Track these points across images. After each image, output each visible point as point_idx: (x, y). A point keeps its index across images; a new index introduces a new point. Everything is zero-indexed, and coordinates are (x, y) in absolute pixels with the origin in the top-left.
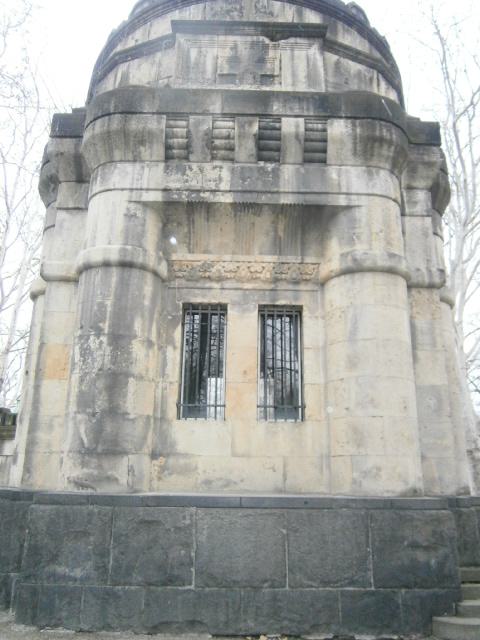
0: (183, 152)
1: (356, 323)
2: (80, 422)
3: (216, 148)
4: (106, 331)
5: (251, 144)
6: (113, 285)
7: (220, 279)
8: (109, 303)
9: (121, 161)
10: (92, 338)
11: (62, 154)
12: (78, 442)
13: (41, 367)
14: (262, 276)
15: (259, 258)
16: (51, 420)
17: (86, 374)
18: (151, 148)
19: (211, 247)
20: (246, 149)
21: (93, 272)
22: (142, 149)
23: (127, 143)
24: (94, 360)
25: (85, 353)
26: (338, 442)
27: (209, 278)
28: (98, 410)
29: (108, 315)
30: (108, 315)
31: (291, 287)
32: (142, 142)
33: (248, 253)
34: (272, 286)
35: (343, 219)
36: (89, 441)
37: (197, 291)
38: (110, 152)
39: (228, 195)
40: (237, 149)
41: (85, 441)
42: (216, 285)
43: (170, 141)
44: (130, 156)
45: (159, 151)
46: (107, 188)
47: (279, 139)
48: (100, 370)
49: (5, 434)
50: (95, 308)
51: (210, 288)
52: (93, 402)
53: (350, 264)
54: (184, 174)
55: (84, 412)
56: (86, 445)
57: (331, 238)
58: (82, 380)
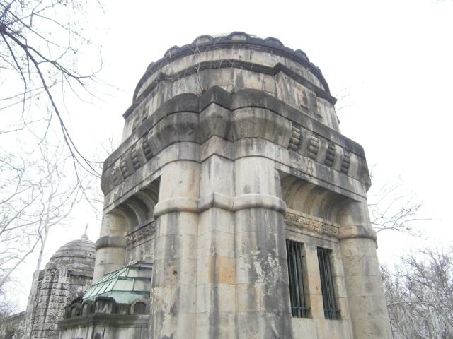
0: (296, 147)
1: (235, 245)
2: (270, 318)
3: (309, 150)
4: (277, 254)
5: (324, 154)
6: (276, 223)
7: (301, 228)
8: (276, 235)
9: (268, 140)
10: (270, 258)
11: (221, 117)
12: (271, 334)
13: (217, 273)
14: (318, 229)
15: (314, 218)
16: (227, 315)
17: (269, 284)
18: (284, 139)
19: (294, 205)
20: (321, 156)
21: (263, 211)
22: (280, 137)
23: (274, 130)
24: (273, 274)
25: (266, 269)
26: (365, 333)
27: (297, 226)
28: (280, 311)
29: (277, 243)
30: (277, 243)
31: (328, 238)
32: (280, 133)
33: (309, 213)
34: (321, 237)
35: (353, 206)
36: (278, 332)
37: (291, 233)
38: (263, 132)
39: (316, 180)
40: (318, 154)
41: (276, 332)
42: (299, 231)
43: (293, 138)
44: (273, 140)
45: (286, 142)
46: (263, 155)
47: (333, 155)
48: (278, 281)
49: (120, 322)
50: (269, 237)
51: (297, 232)
52: (277, 303)
53: (362, 233)
54: (297, 160)
55: (272, 311)
56: (277, 336)
57: (346, 215)
58: (266, 287)
